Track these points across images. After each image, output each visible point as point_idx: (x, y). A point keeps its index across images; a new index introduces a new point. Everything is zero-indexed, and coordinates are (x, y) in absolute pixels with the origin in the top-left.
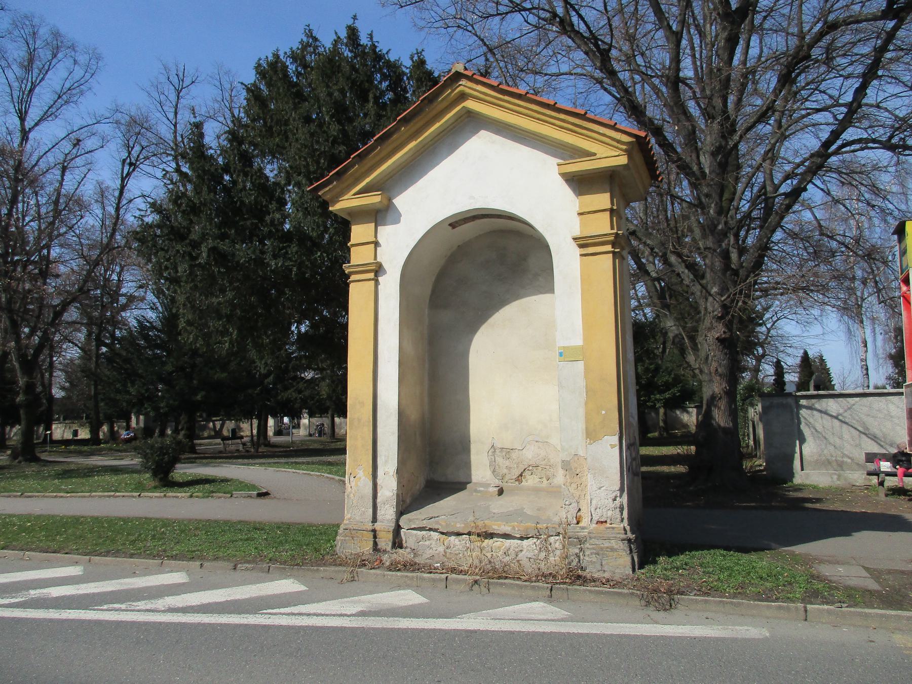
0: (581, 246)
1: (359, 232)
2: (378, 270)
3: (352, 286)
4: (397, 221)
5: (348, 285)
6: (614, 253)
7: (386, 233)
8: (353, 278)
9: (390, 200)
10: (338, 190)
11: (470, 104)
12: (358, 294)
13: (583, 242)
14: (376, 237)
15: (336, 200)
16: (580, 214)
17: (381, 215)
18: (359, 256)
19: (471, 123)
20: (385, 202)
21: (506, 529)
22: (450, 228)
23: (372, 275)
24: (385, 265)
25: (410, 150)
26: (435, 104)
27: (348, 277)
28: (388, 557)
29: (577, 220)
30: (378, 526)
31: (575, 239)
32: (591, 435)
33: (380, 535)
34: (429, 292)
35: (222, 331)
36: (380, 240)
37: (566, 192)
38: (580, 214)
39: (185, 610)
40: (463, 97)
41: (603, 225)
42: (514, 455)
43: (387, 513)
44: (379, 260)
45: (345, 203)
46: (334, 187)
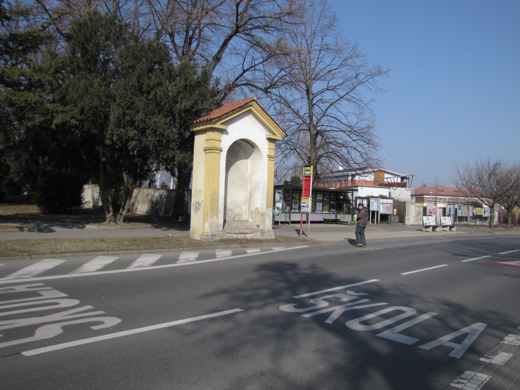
7: (224, 137)
11: (252, 108)
13: (269, 157)
19: (250, 112)
21: (247, 232)
29: (268, 150)
32: (268, 207)
37: (266, 141)
40: (252, 105)
42: (233, 211)
44: (221, 147)
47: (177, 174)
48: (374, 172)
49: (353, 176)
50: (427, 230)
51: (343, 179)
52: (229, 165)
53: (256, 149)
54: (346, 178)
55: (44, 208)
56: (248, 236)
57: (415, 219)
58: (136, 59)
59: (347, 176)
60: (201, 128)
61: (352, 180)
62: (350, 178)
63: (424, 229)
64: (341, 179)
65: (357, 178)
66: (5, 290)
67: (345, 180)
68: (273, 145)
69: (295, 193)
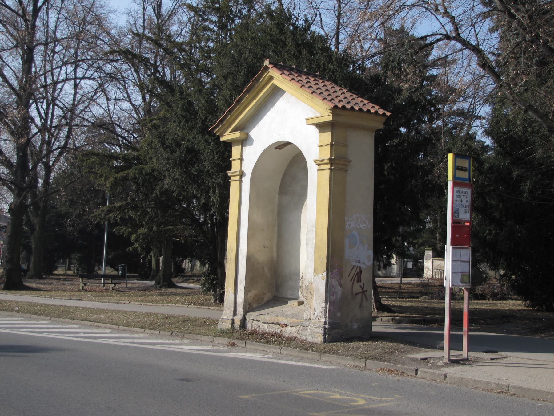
0: (319, 165)
1: (235, 151)
2: (242, 174)
3: (231, 183)
4: (252, 144)
5: (230, 182)
6: (331, 169)
8: (232, 178)
9: (247, 134)
10: (222, 130)
12: (234, 187)
14: (241, 156)
15: (222, 135)
16: (319, 146)
17: (244, 141)
18: (235, 166)
19: (277, 92)
20: (244, 136)
22: (278, 150)
23: (238, 178)
24: (245, 172)
25: (252, 107)
26: (259, 83)
27: (230, 178)
28: (241, 333)
30: (235, 318)
31: (314, 161)
32: (316, 272)
33: (235, 322)
34: (279, 183)
35: (149, 215)
36: (244, 157)
38: (319, 146)
39: (126, 342)
41: (326, 154)
43: (240, 310)
45: (227, 137)
46: (221, 128)
56: (289, 331)
68: (327, 137)
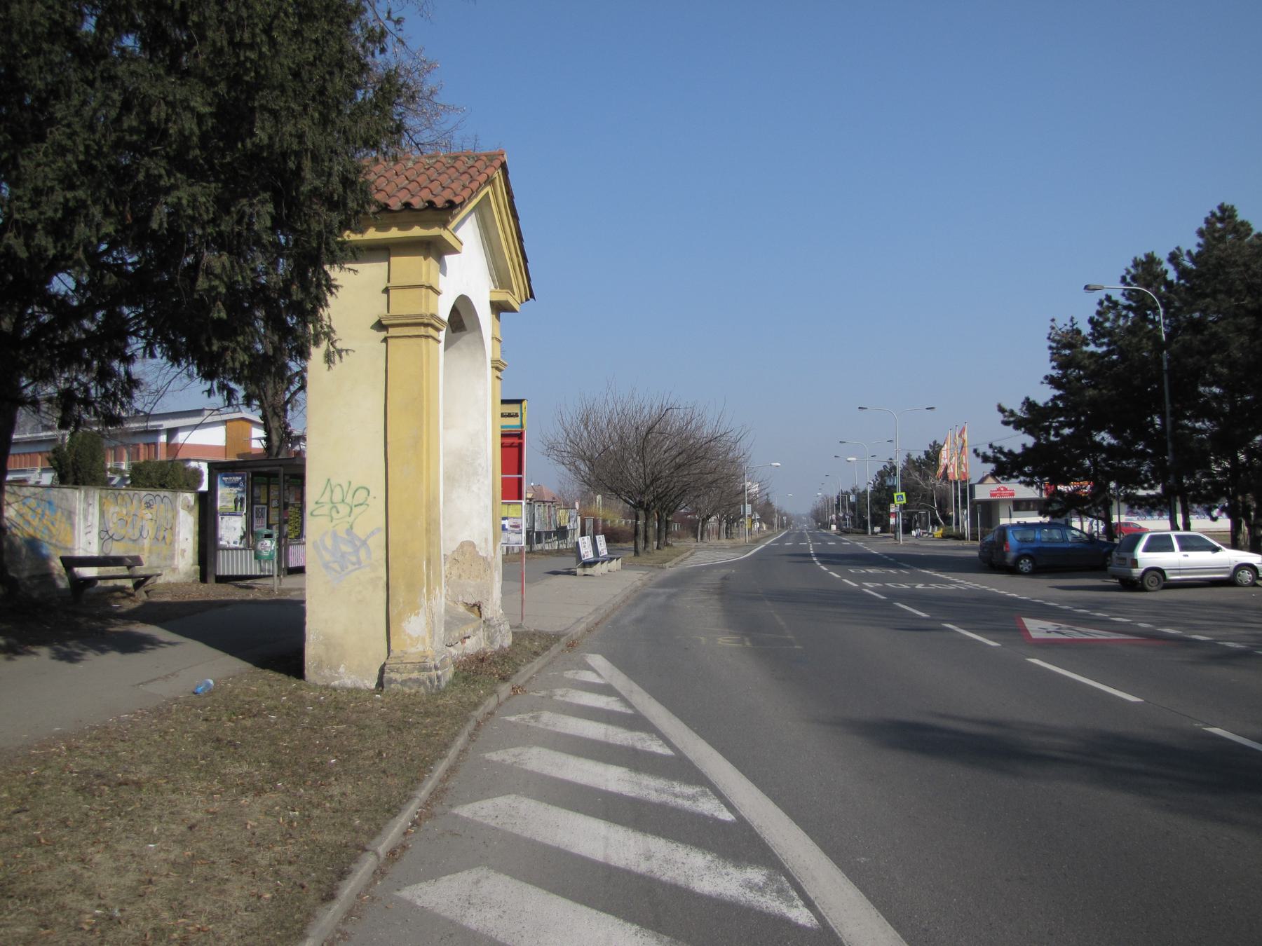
47: (1218, 545)
48: (225, 422)
49: (172, 432)
50: (589, 571)
51: (141, 441)
52: (446, 349)
53: (467, 337)
54: (150, 440)
55: (1194, 259)
57: (1054, 364)
58: (296, 75)
59: (156, 432)
60: (372, 234)
61: (168, 444)
62: (163, 438)
63: (579, 571)
64: (136, 440)
65: (181, 438)
66: (512, 260)
67: (148, 444)
69: (260, 484)
